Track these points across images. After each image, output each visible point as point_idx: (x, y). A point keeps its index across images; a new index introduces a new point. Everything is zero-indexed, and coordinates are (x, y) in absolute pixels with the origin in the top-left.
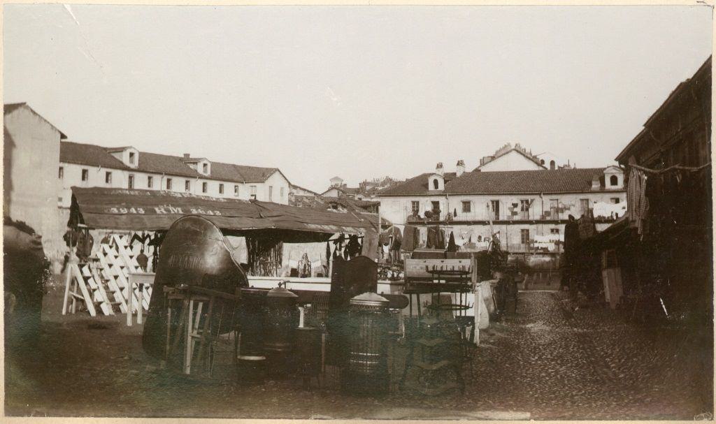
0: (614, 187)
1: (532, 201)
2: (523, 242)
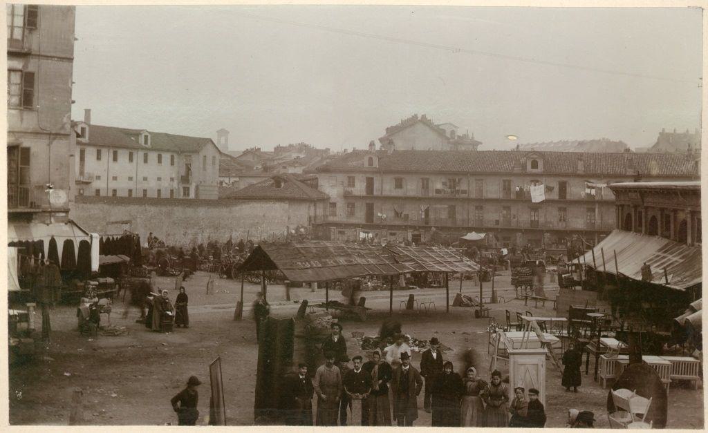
0: (534, 171)
1: (459, 180)
2: (450, 217)
